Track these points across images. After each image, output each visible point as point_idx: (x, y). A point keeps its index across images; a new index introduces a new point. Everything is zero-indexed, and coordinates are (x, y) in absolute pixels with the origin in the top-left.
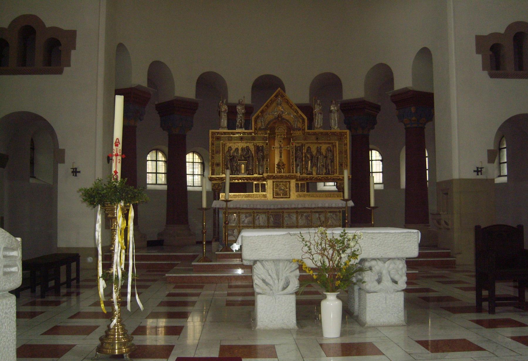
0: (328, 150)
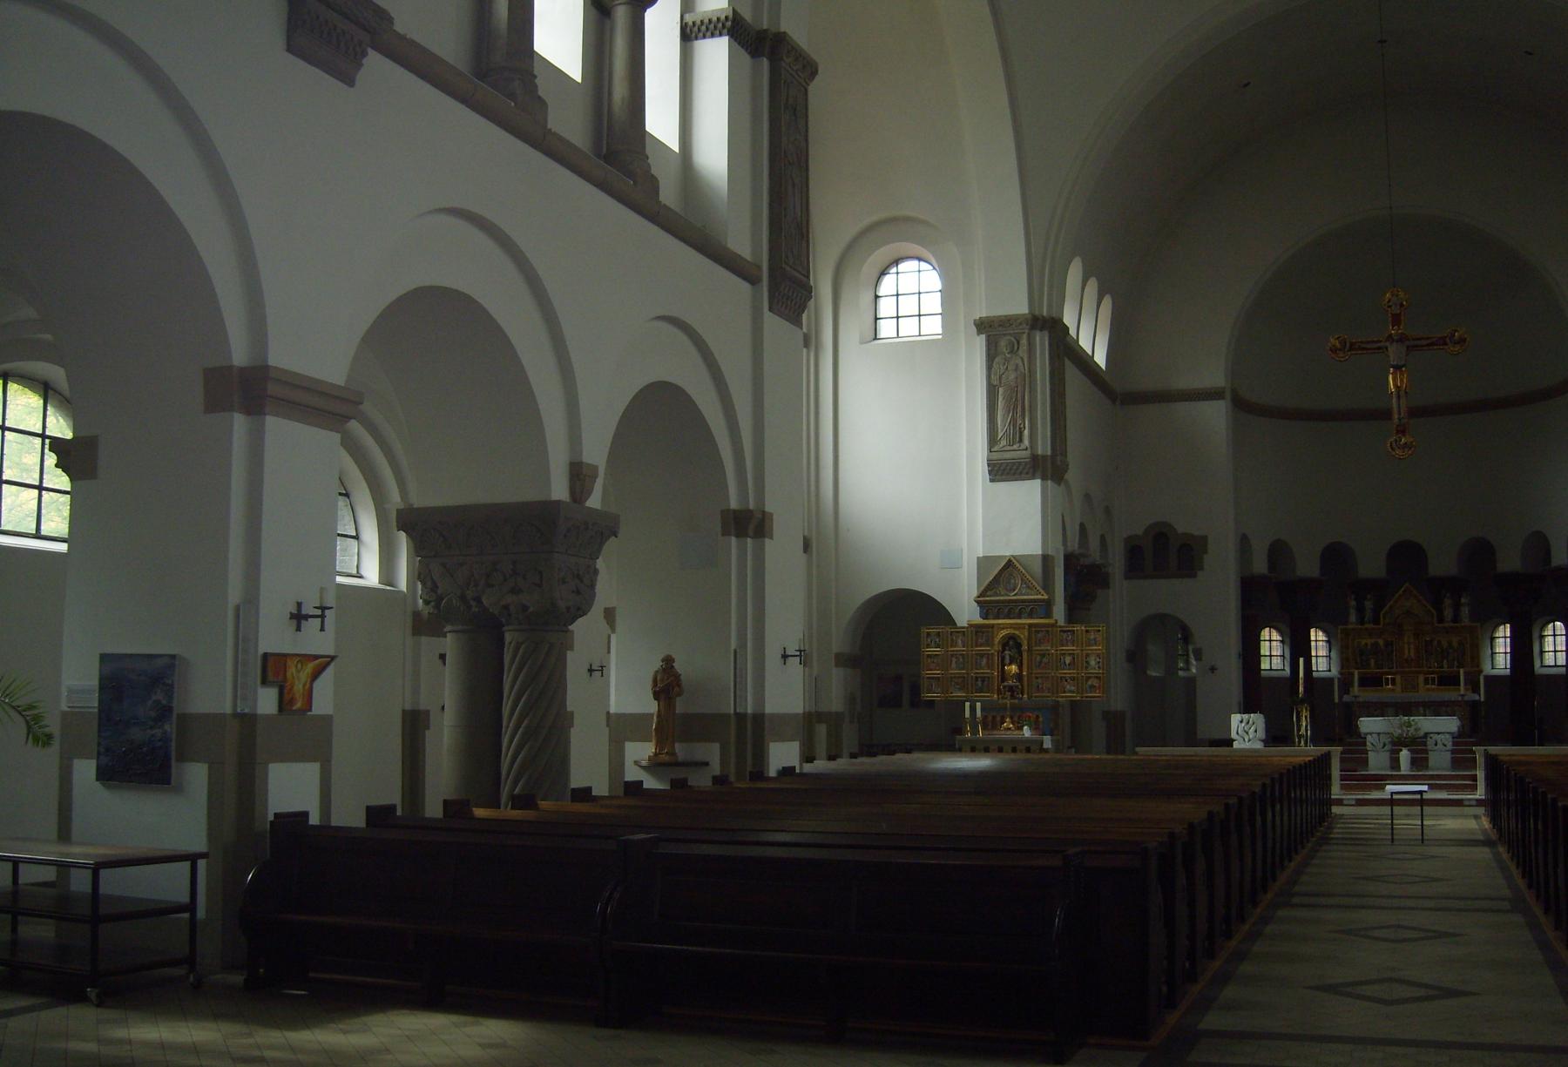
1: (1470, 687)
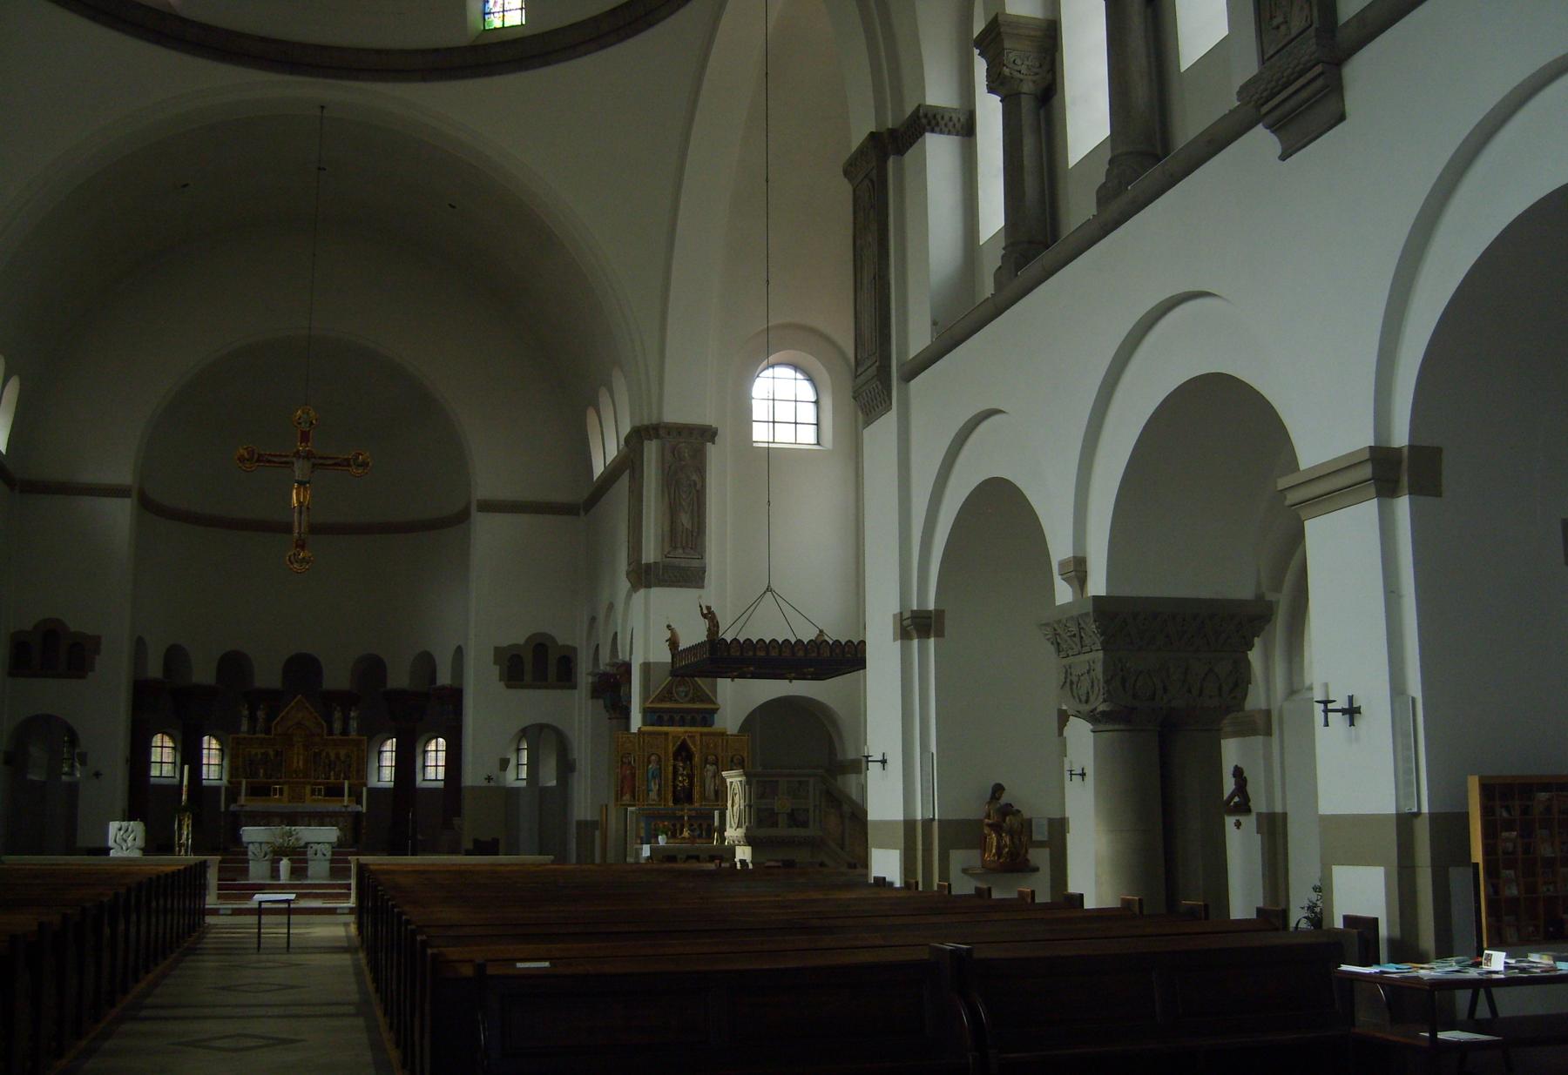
0: (348, 756)
1: (354, 798)
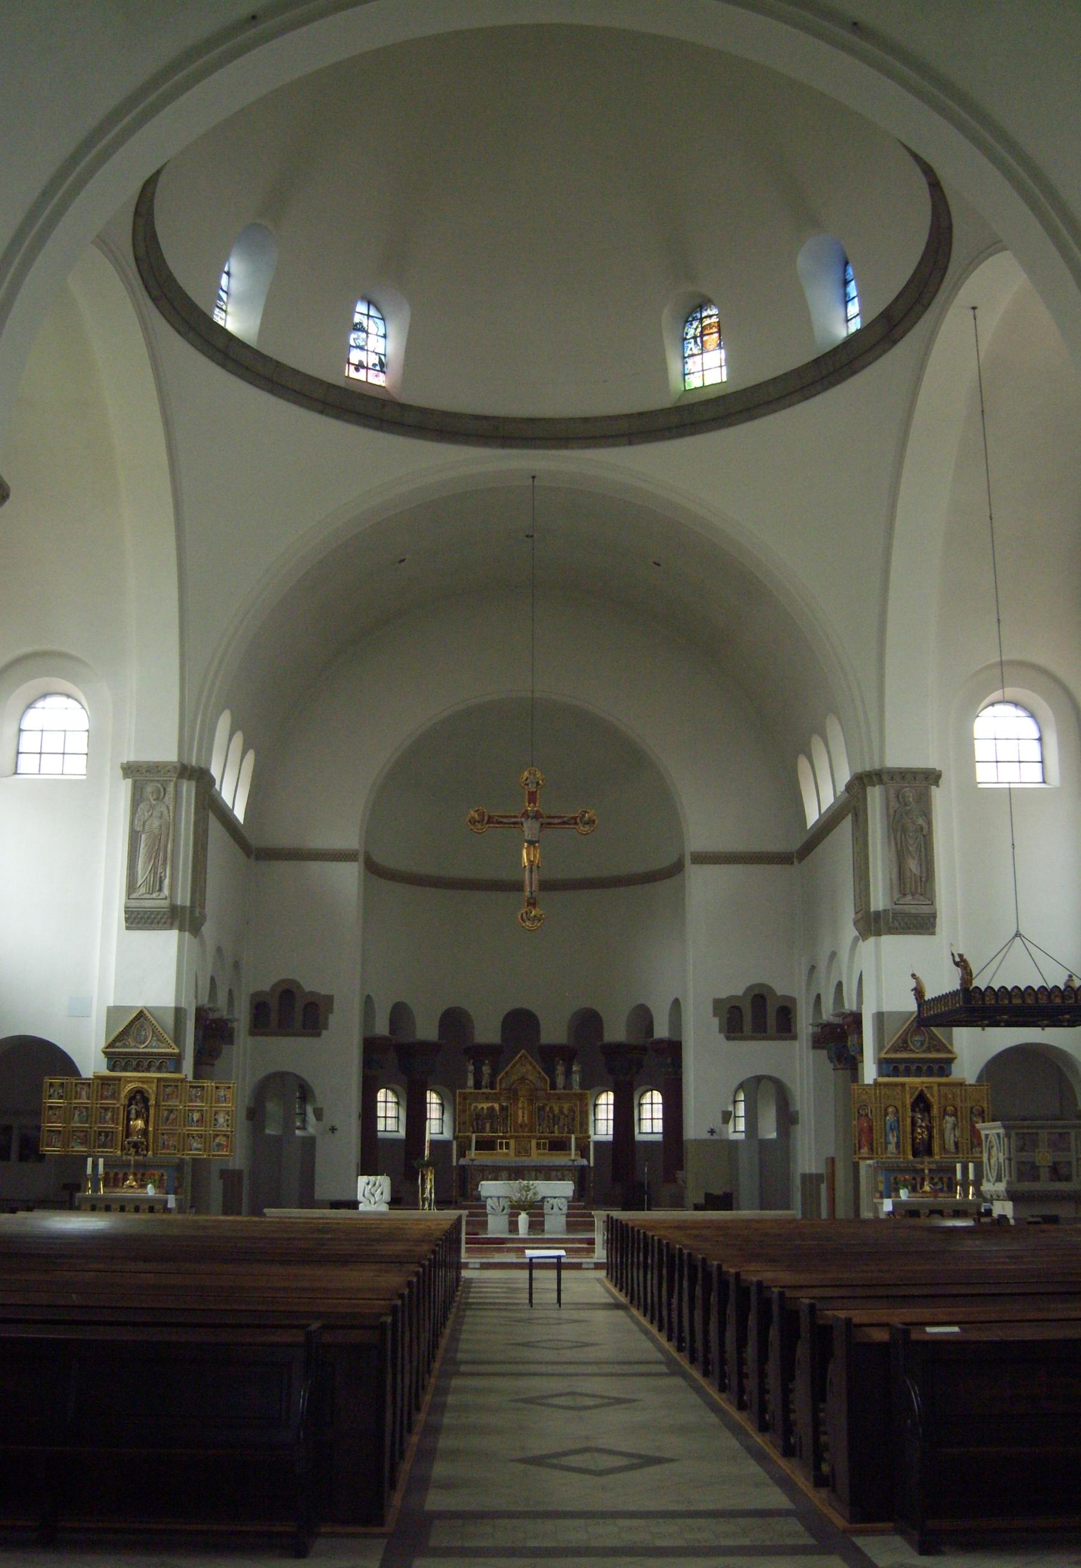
0: (571, 1110)
1: (579, 1153)
